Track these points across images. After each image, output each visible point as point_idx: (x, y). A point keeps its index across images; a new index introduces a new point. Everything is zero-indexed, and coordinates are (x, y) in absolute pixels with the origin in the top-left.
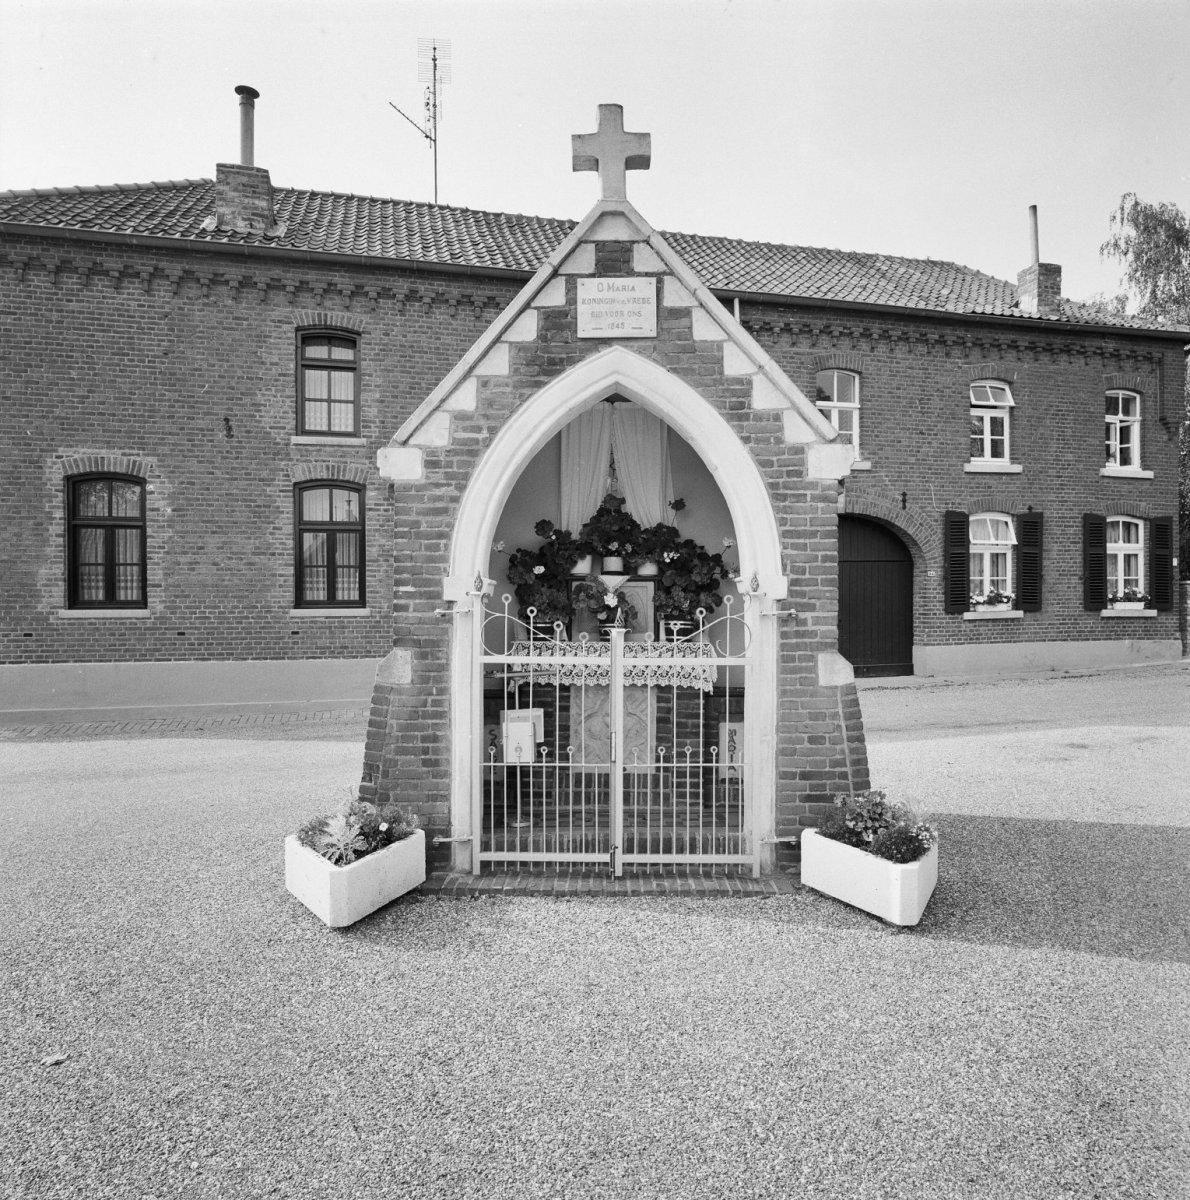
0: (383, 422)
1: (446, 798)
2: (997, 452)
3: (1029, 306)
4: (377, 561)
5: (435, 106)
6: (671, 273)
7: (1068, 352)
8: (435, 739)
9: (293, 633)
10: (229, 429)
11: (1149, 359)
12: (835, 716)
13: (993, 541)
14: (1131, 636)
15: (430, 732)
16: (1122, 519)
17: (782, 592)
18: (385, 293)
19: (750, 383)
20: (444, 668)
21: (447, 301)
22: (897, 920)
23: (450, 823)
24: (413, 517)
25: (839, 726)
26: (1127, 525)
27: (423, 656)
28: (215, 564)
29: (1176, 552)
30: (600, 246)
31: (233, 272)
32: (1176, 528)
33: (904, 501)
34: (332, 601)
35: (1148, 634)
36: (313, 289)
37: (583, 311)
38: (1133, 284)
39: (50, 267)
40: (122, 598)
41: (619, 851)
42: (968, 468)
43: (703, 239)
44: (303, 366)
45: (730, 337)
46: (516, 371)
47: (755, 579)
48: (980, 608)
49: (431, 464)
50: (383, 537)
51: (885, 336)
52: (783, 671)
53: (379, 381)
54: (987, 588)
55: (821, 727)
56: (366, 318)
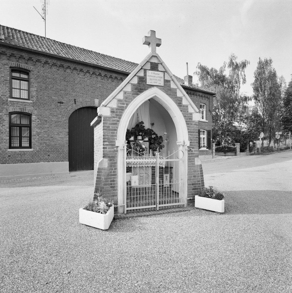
0: (37, 97)
1: (116, 196)
4: (36, 135)
5: (45, 10)
7: (194, 94)
8: (114, 181)
9: (9, 156)
11: (207, 98)
14: (204, 154)
15: (112, 179)
16: (203, 130)
17: (188, 145)
18: (38, 61)
19: (182, 98)
21: (56, 65)
22: (103, 229)
23: (117, 202)
24: (108, 125)
25: (199, 173)
26: (203, 131)
30: (152, 63)
34: (21, 147)
35: (207, 154)
36: (16, 56)
37: (148, 78)
38: (200, 81)
41: (158, 204)
44: (12, 78)
45: (178, 88)
46: (133, 90)
47: (184, 141)
49: (112, 112)
50: (37, 129)
52: (189, 162)
53: (36, 85)
55: (196, 174)
56: (32, 67)
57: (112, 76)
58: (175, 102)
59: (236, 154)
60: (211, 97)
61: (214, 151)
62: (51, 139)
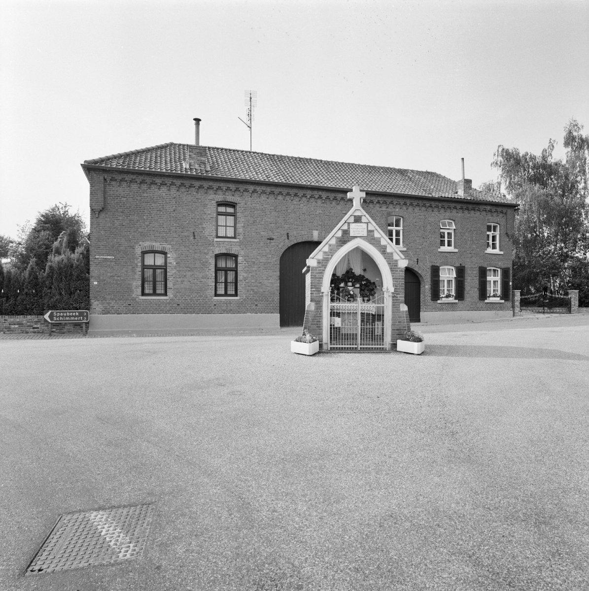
1: (322, 334)
2: (449, 245)
3: (461, 194)
5: (251, 115)
6: (370, 222)
7: (474, 210)
10: (194, 236)
11: (502, 212)
12: (404, 317)
13: (448, 276)
14: (495, 309)
16: (492, 268)
18: (246, 190)
19: (386, 246)
20: (322, 306)
26: (494, 271)
27: (316, 304)
28: (190, 281)
29: (511, 280)
31: (197, 184)
32: (511, 272)
33: (418, 262)
34: (226, 294)
37: (351, 231)
39: (138, 182)
40: (158, 293)
42: (440, 250)
43: (346, 164)
45: (382, 237)
48: (443, 299)
49: (319, 263)
51: (411, 204)
52: (393, 307)
53: (243, 220)
54: (446, 292)
56: (239, 199)
57: (337, 198)
58: (379, 250)
59: (570, 312)
60: (509, 211)
61: (517, 304)
62: (260, 285)
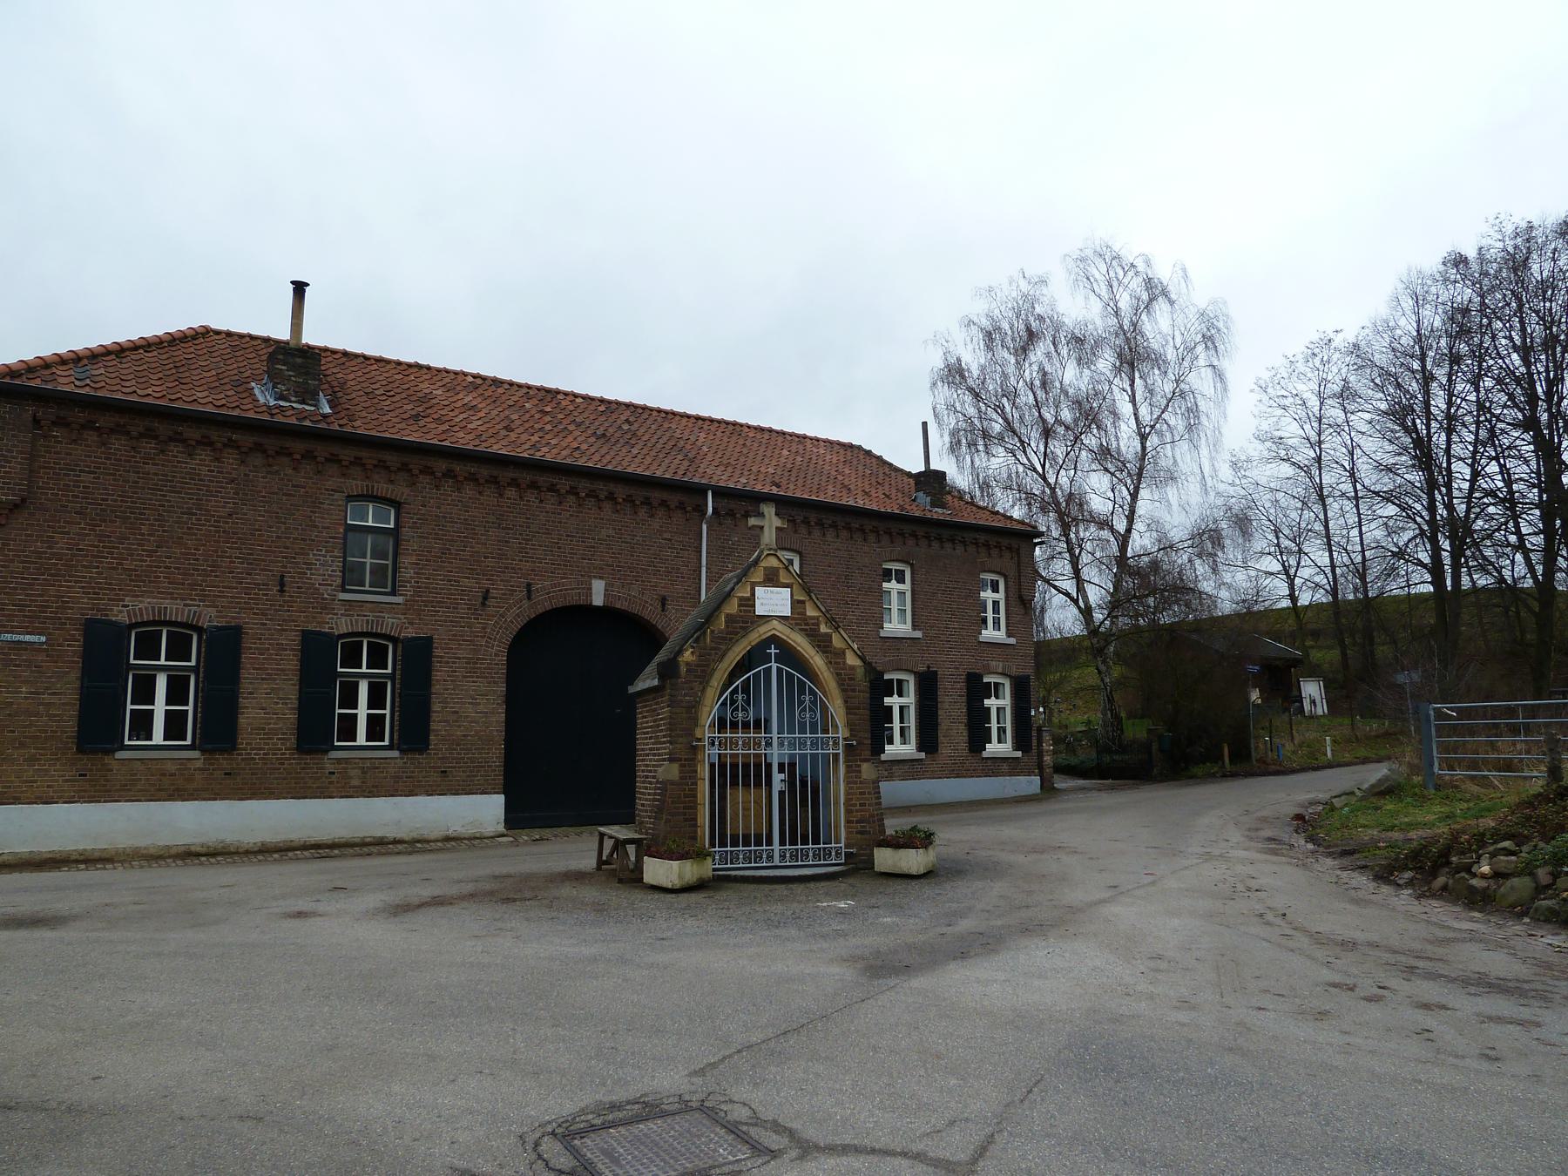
7: (953, 541)
11: (1010, 548)
56: (407, 491)
